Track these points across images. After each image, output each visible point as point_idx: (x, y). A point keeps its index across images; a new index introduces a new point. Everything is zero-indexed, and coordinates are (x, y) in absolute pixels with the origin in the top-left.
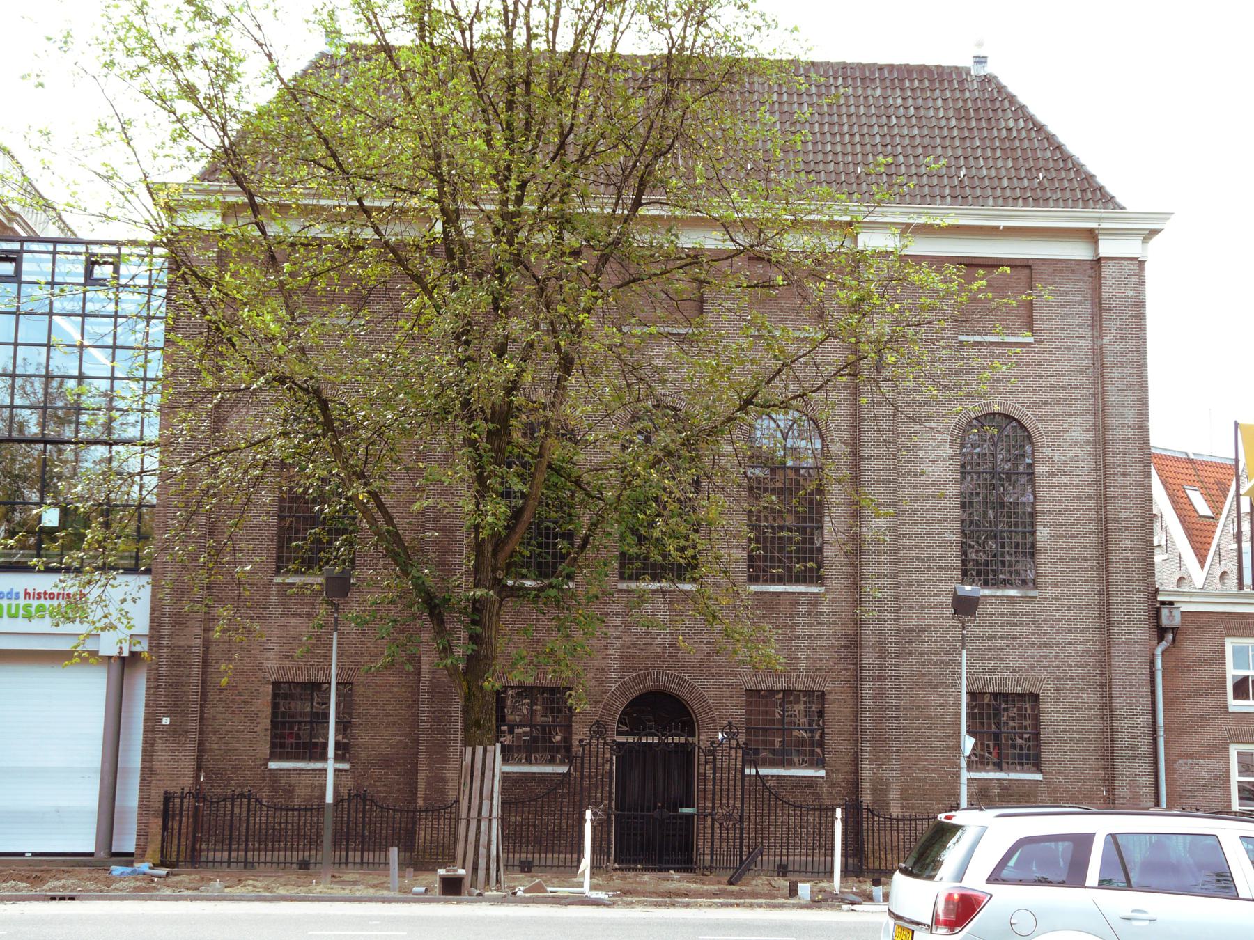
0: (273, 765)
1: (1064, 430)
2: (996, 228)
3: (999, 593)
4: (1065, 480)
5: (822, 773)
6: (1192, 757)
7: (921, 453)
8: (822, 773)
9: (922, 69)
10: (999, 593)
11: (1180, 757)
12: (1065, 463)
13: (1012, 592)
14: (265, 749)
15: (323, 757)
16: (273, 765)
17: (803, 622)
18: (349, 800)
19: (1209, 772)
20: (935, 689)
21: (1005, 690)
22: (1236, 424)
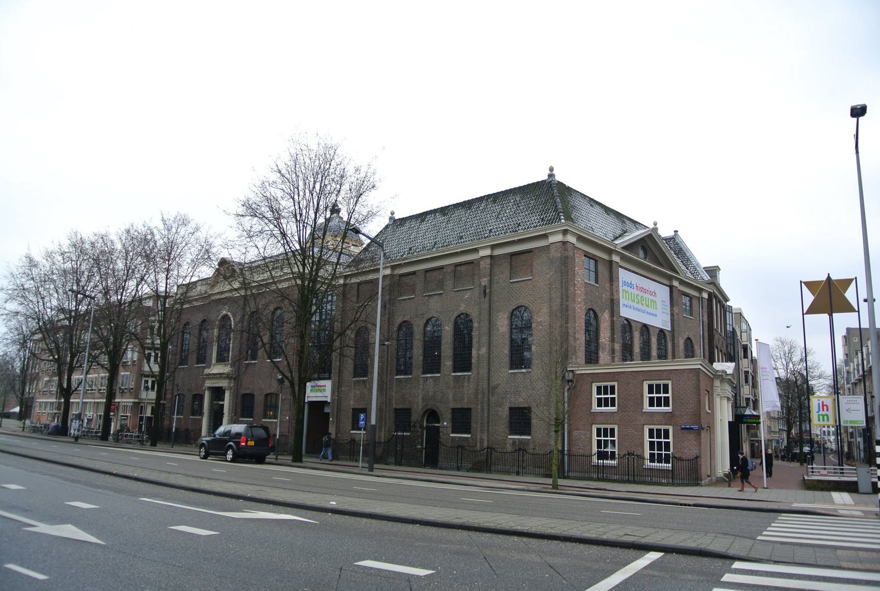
0: (352, 432)
1: (541, 309)
2: (514, 241)
3: (520, 371)
4: (541, 327)
5: (470, 436)
6: (579, 430)
7: (499, 323)
8: (470, 436)
9: (502, 192)
10: (520, 371)
11: (575, 430)
12: (541, 321)
13: (524, 371)
14: (350, 428)
15: (654, 442)
16: (352, 432)
17: (466, 384)
18: (487, 448)
19: (584, 435)
20: (501, 407)
21: (521, 406)
22: (801, 282)
